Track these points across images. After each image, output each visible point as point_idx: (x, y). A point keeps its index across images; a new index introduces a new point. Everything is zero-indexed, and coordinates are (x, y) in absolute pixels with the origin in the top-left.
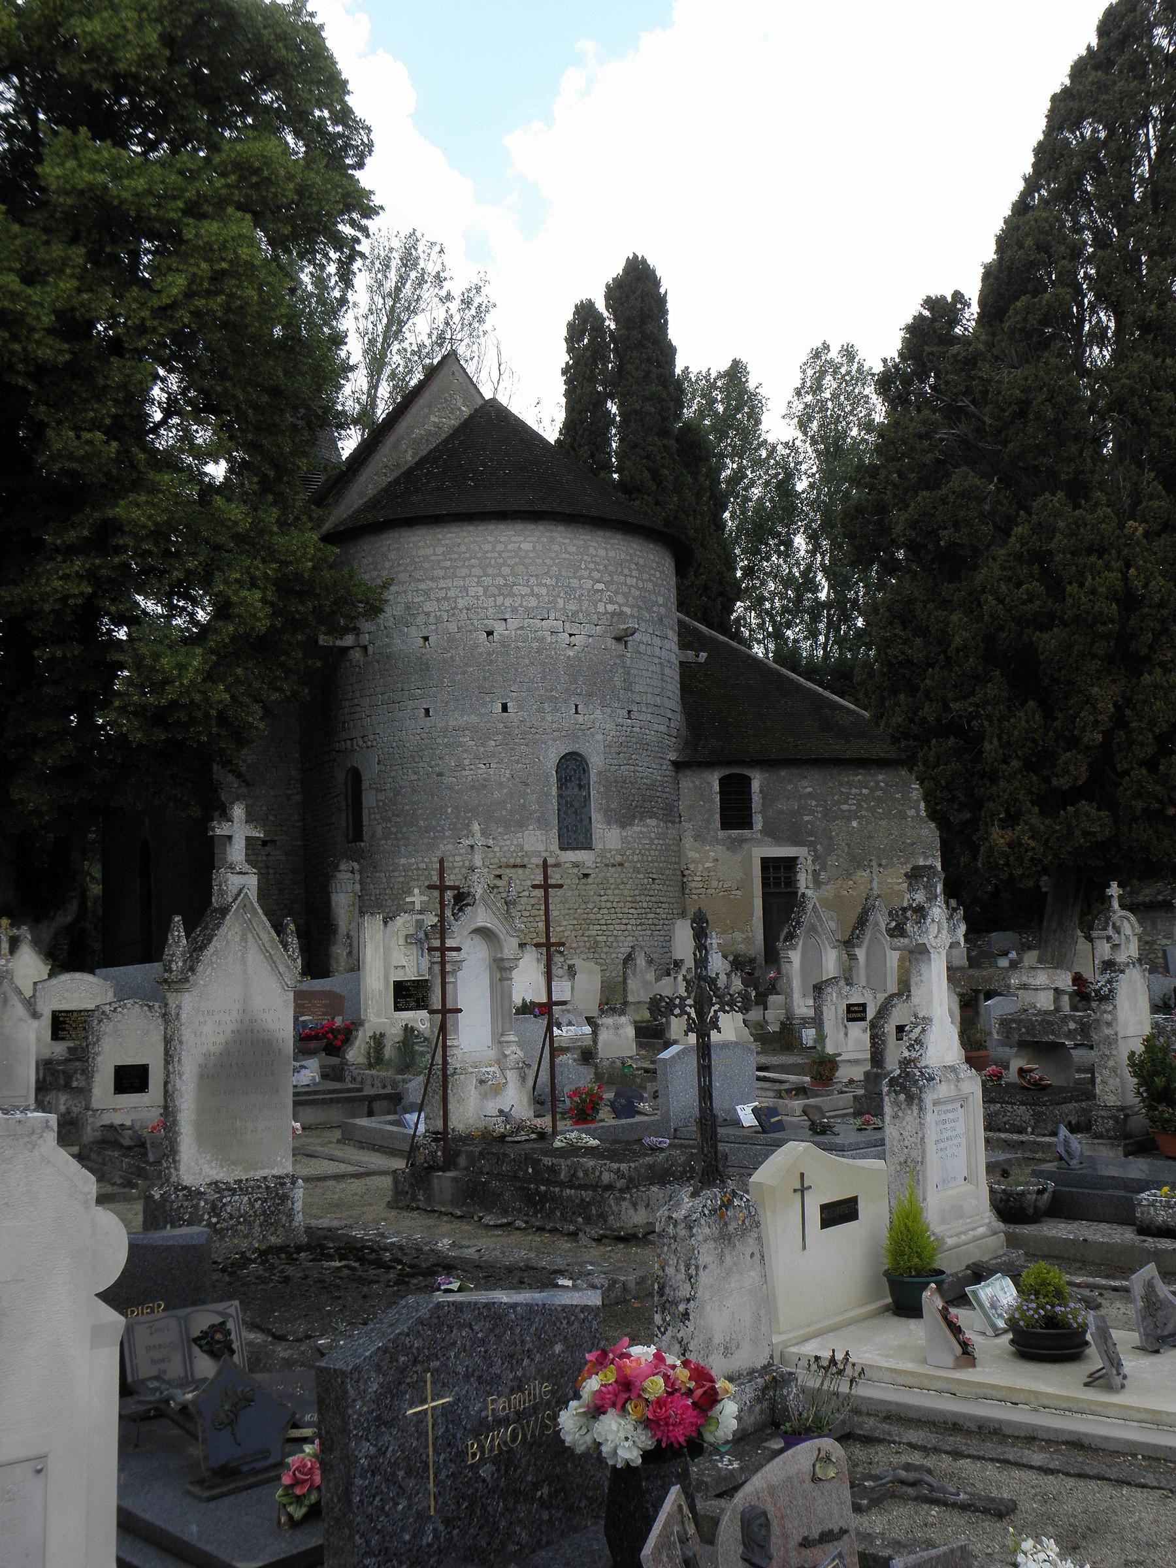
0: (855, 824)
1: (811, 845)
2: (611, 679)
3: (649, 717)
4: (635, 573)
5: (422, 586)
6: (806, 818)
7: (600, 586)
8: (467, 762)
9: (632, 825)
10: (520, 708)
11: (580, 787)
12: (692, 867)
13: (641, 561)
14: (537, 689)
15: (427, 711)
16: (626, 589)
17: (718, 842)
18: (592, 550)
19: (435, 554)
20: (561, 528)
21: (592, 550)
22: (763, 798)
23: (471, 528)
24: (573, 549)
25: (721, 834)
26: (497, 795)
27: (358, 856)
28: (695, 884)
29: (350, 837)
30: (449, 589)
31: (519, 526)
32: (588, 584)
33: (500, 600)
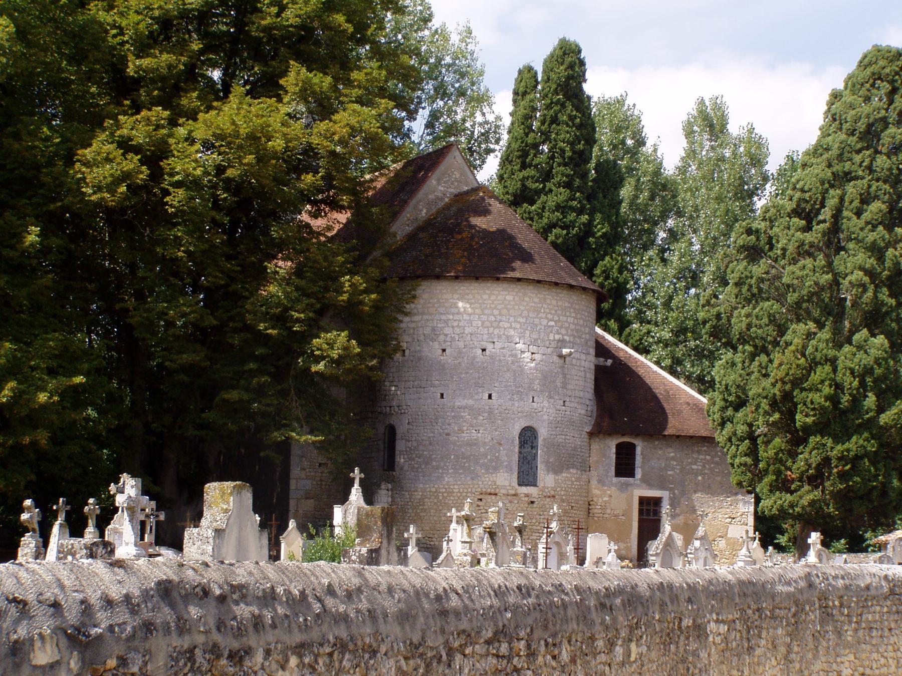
0: (700, 478)
1: (671, 490)
2: (554, 382)
3: (576, 405)
4: (573, 315)
5: (443, 317)
6: (669, 473)
7: (552, 323)
8: (465, 428)
9: (562, 472)
10: (500, 397)
11: (532, 447)
12: (595, 499)
13: (577, 307)
14: (510, 386)
15: (442, 395)
16: (567, 325)
17: (612, 485)
18: (548, 301)
19: (453, 298)
20: (531, 287)
21: (548, 301)
22: (643, 458)
23: (476, 285)
24: (536, 300)
25: (615, 480)
26: (482, 450)
27: (391, 480)
28: (596, 510)
29: (386, 467)
30: (460, 321)
31: (505, 285)
32: (545, 322)
33: (491, 330)
